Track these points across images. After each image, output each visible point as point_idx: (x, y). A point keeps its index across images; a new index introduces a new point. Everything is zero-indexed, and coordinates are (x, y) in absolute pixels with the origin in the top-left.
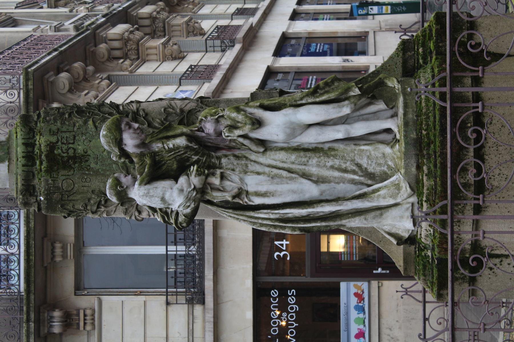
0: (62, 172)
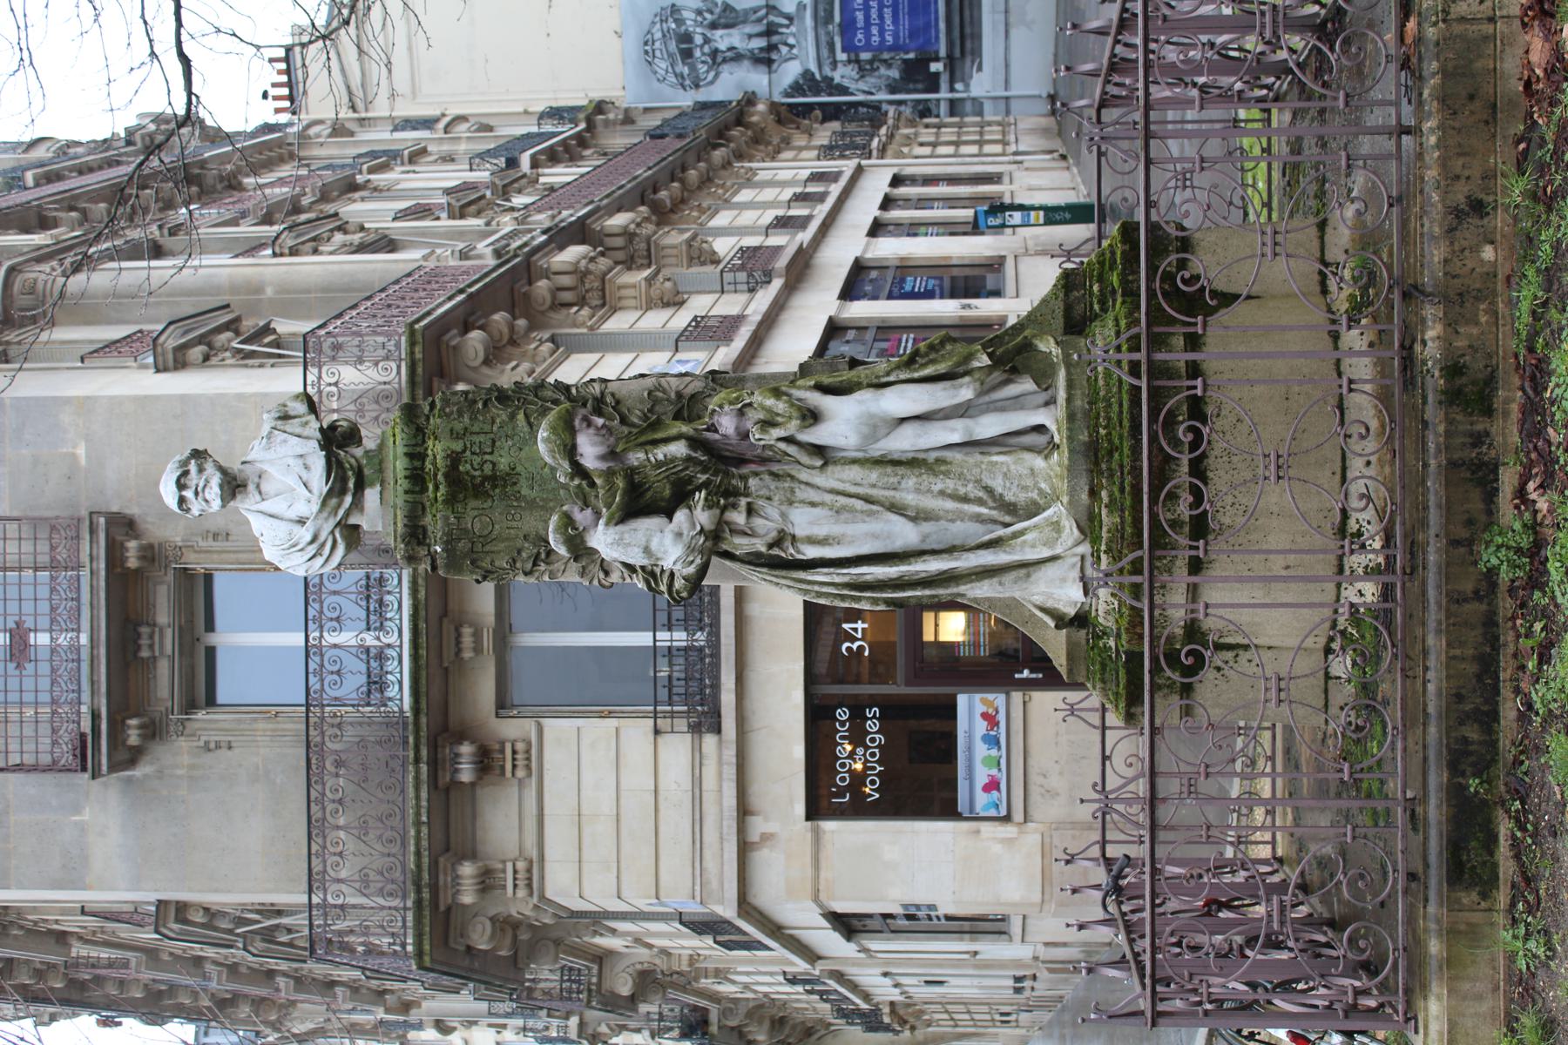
0: (473, 503)
